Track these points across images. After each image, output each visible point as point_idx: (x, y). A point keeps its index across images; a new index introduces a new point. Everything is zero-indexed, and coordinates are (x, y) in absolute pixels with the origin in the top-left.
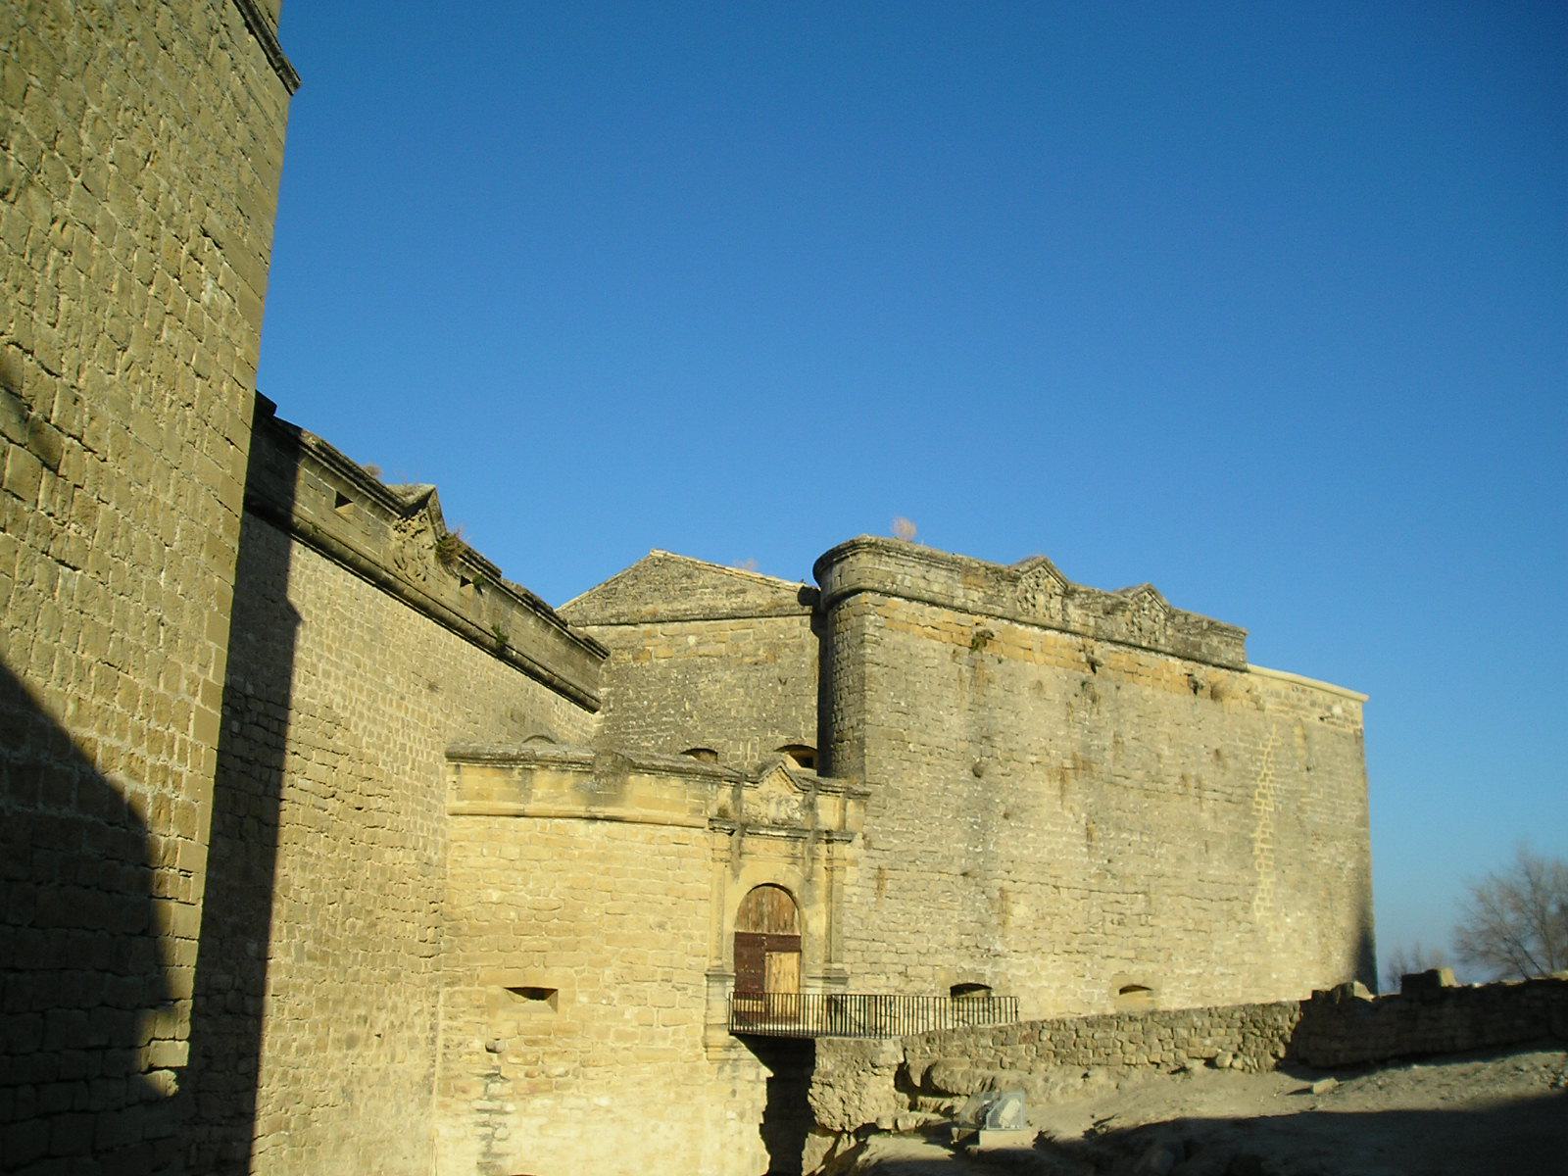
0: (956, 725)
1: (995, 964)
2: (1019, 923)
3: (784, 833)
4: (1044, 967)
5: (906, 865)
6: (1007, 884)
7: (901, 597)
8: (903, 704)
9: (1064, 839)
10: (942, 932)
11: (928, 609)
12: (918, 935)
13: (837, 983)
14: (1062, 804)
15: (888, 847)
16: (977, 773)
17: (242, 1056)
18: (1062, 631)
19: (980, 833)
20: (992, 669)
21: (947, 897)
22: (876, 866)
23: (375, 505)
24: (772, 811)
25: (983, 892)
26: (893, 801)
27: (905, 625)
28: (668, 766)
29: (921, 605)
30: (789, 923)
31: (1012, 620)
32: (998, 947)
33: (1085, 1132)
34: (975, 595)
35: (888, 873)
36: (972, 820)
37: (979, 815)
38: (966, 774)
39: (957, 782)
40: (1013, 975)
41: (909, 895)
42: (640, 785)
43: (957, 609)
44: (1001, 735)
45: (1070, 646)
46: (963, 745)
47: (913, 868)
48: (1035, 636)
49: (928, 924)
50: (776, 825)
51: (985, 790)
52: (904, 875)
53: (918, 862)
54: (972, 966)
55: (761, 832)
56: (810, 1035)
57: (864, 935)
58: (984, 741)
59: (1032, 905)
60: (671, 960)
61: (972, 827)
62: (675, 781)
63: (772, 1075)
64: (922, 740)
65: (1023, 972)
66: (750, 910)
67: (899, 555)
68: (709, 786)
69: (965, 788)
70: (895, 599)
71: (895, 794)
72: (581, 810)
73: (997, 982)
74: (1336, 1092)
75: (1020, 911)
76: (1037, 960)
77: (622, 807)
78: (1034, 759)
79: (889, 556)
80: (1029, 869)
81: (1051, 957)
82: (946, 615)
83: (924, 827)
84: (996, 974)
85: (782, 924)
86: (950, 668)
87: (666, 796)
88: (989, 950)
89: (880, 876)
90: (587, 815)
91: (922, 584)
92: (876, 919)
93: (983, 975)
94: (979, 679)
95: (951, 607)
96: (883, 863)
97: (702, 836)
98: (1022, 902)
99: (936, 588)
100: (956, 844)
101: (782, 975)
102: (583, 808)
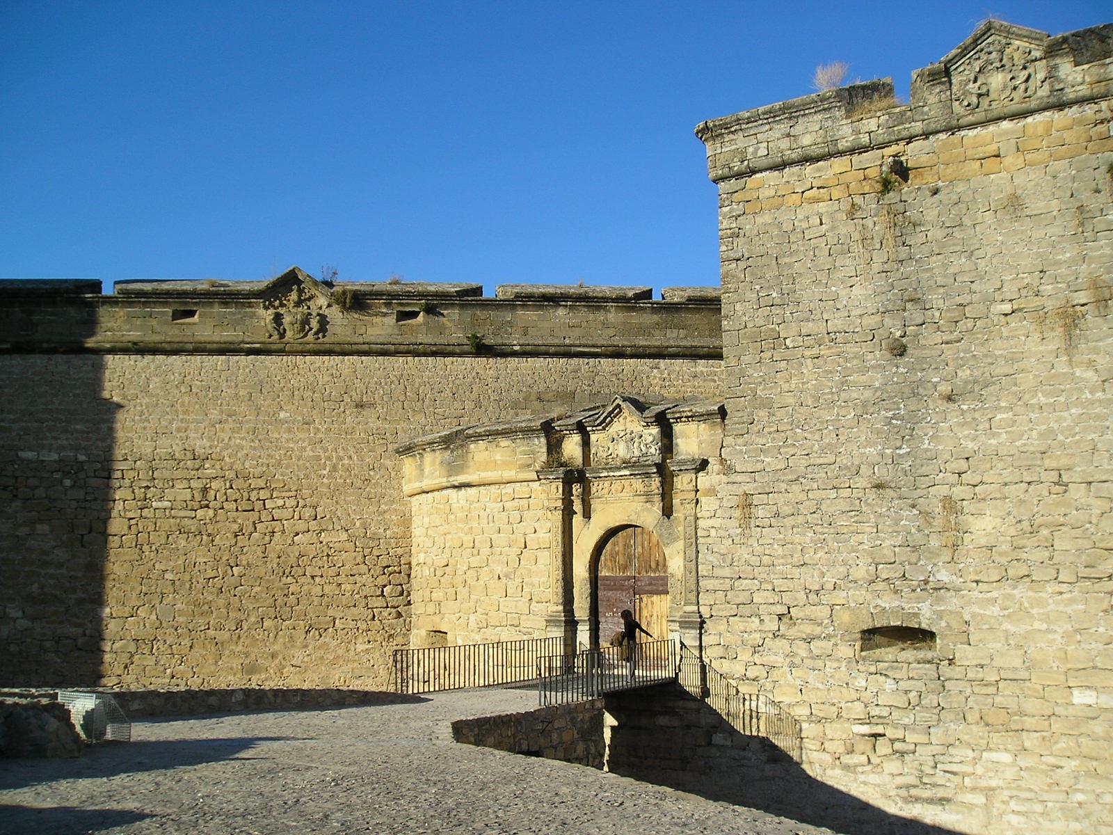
0: (858, 297)
1: (939, 600)
2: (983, 542)
3: (628, 473)
4: (1041, 603)
5: (783, 486)
6: (958, 492)
7: (761, 171)
8: (774, 295)
9: (1073, 411)
10: (844, 563)
11: (809, 169)
12: (803, 569)
13: (687, 628)
14: (1070, 360)
15: (759, 467)
16: (900, 350)
17: (325, 693)
18: (1061, 106)
19: (905, 429)
20: (929, 210)
21: (851, 517)
22: (740, 492)
23: (219, 303)
24: (621, 450)
25: (914, 506)
26: (763, 413)
27: (777, 201)
28: (488, 431)
29: (796, 169)
30: (661, 563)
31: (952, 129)
32: (944, 576)
33: (87, 712)
34: (872, 124)
35: (756, 500)
36: (890, 414)
37: (902, 406)
38: (879, 356)
39: (864, 370)
40: (974, 615)
41: (789, 522)
42: (479, 451)
43: (852, 151)
44: (941, 290)
45: (1079, 122)
46: (870, 321)
47: (796, 488)
48: (1006, 133)
49: (820, 554)
50: (627, 464)
51: (912, 370)
52: (780, 499)
53: (802, 480)
54: (896, 603)
55: (601, 475)
56: (641, 684)
57: (727, 572)
58: (909, 305)
59: (1009, 514)
60: (516, 606)
61: (890, 423)
62: (504, 442)
63: (616, 723)
64: (804, 331)
65: (995, 610)
66: (617, 553)
67: (744, 126)
68: (536, 440)
69: (875, 371)
70: (758, 175)
71: (768, 404)
72: (444, 481)
73: (943, 624)
74: (766, 748)
75: (984, 525)
76: (1021, 592)
77: (464, 474)
78: (1007, 308)
79: (732, 133)
80: (1000, 465)
81: (1052, 588)
82: (839, 164)
83: (809, 436)
84: (940, 615)
85: (653, 566)
86: (847, 228)
87: (498, 457)
88: (926, 582)
89: (746, 504)
90: (449, 485)
91: (785, 144)
92: (743, 553)
93: (916, 615)
94: (902, 225)
95: (841, 153)
96: (749, 488)
97: (540, 488)
98: (988, 513)
99: (806, 140)
100: (866, 448)
101: (655, 617)
102: (445, 480)
